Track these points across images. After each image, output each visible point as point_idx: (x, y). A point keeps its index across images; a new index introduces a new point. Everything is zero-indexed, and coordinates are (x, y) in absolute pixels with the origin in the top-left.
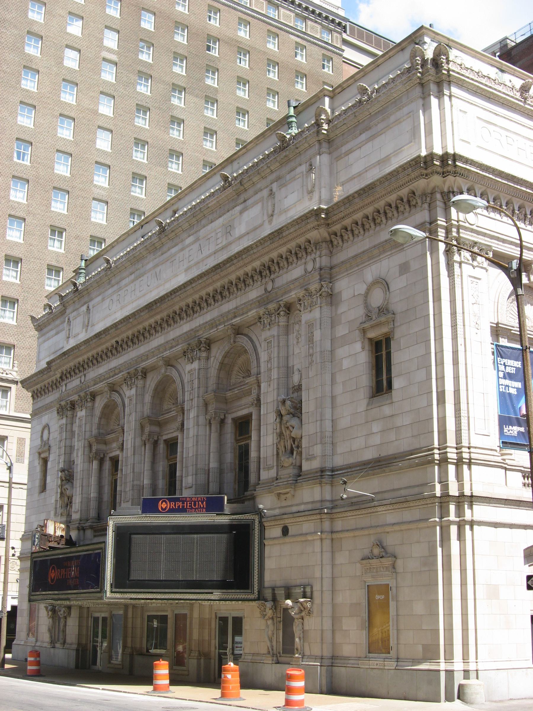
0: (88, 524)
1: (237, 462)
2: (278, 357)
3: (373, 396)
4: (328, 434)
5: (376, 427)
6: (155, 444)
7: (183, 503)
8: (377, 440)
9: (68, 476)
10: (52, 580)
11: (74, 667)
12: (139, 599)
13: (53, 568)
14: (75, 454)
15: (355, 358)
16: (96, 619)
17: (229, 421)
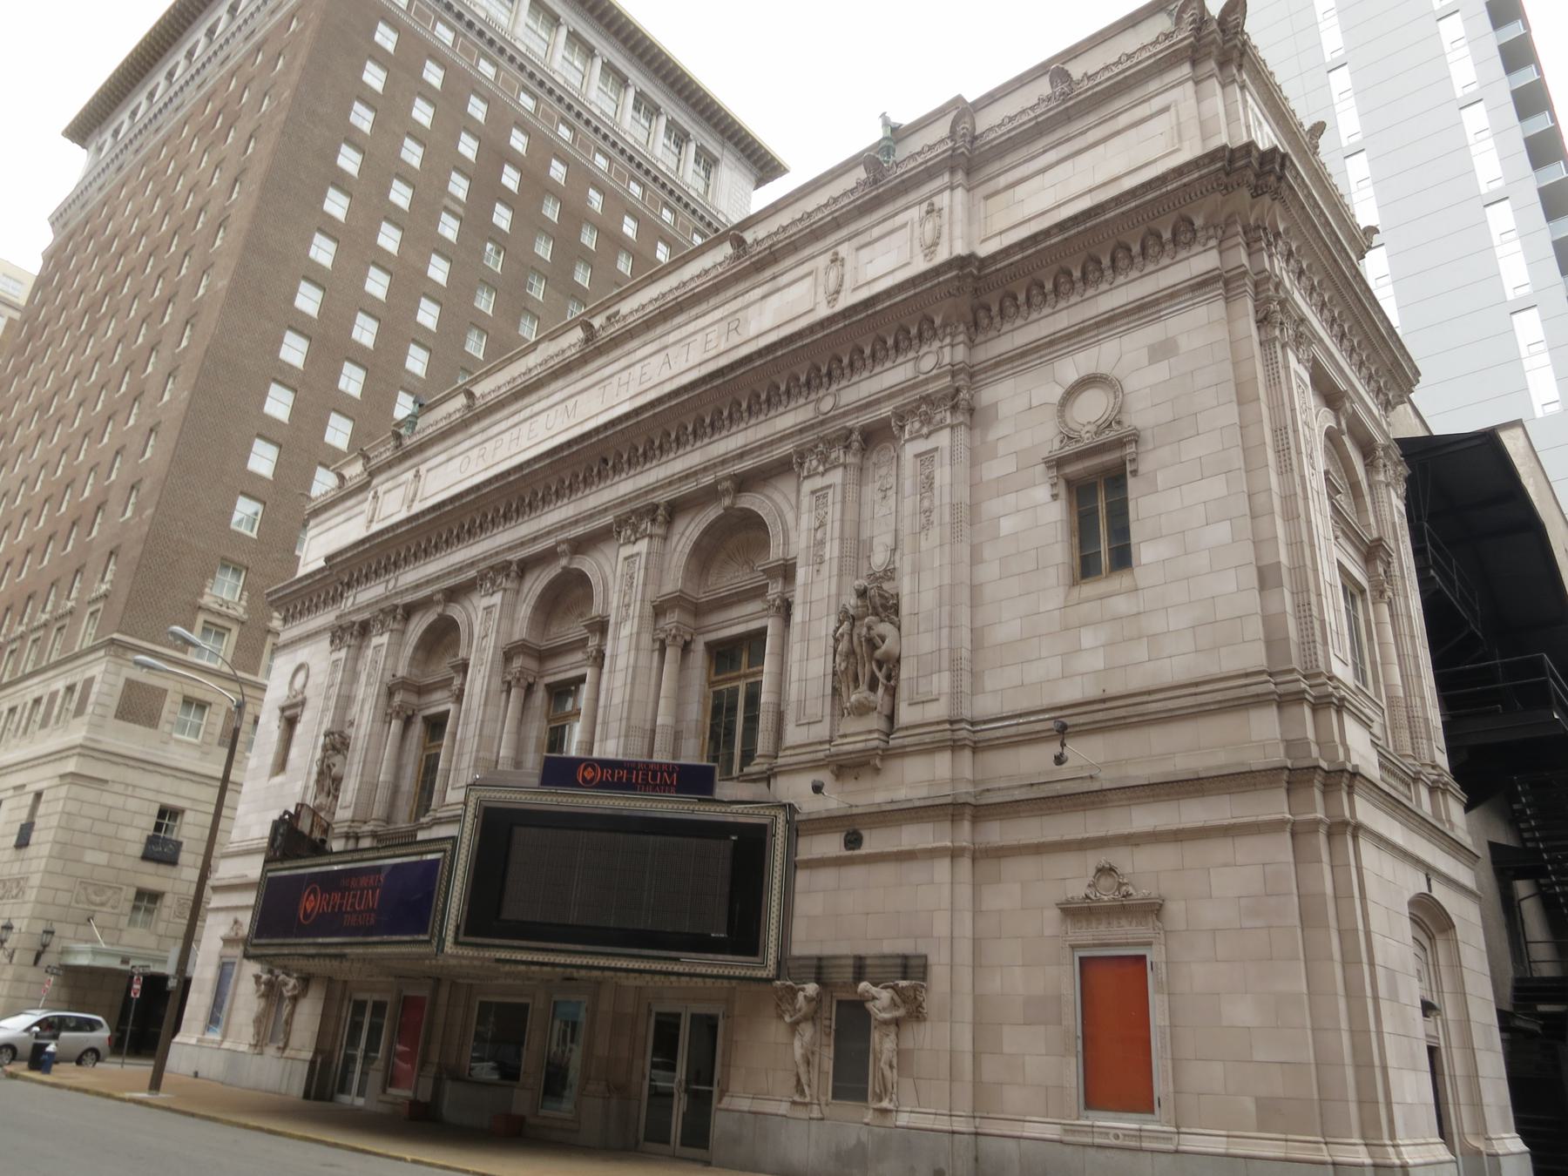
0: (366, 828)
1: (708, 721)
2: (842, 521)
3: (1074, 583)
4: (965, 654)
5: (1088, 638)
6: (529, 690)
7: (630, 772)
8: (1096, 661)
9: (337, 743)
10: (306, 916)
11: (301, 1094)
12: (516, 962)
13: (314, 891)
14: (355, 709)
15: (1037, 516)
16: (359, 1007)
17: (699, 648)
